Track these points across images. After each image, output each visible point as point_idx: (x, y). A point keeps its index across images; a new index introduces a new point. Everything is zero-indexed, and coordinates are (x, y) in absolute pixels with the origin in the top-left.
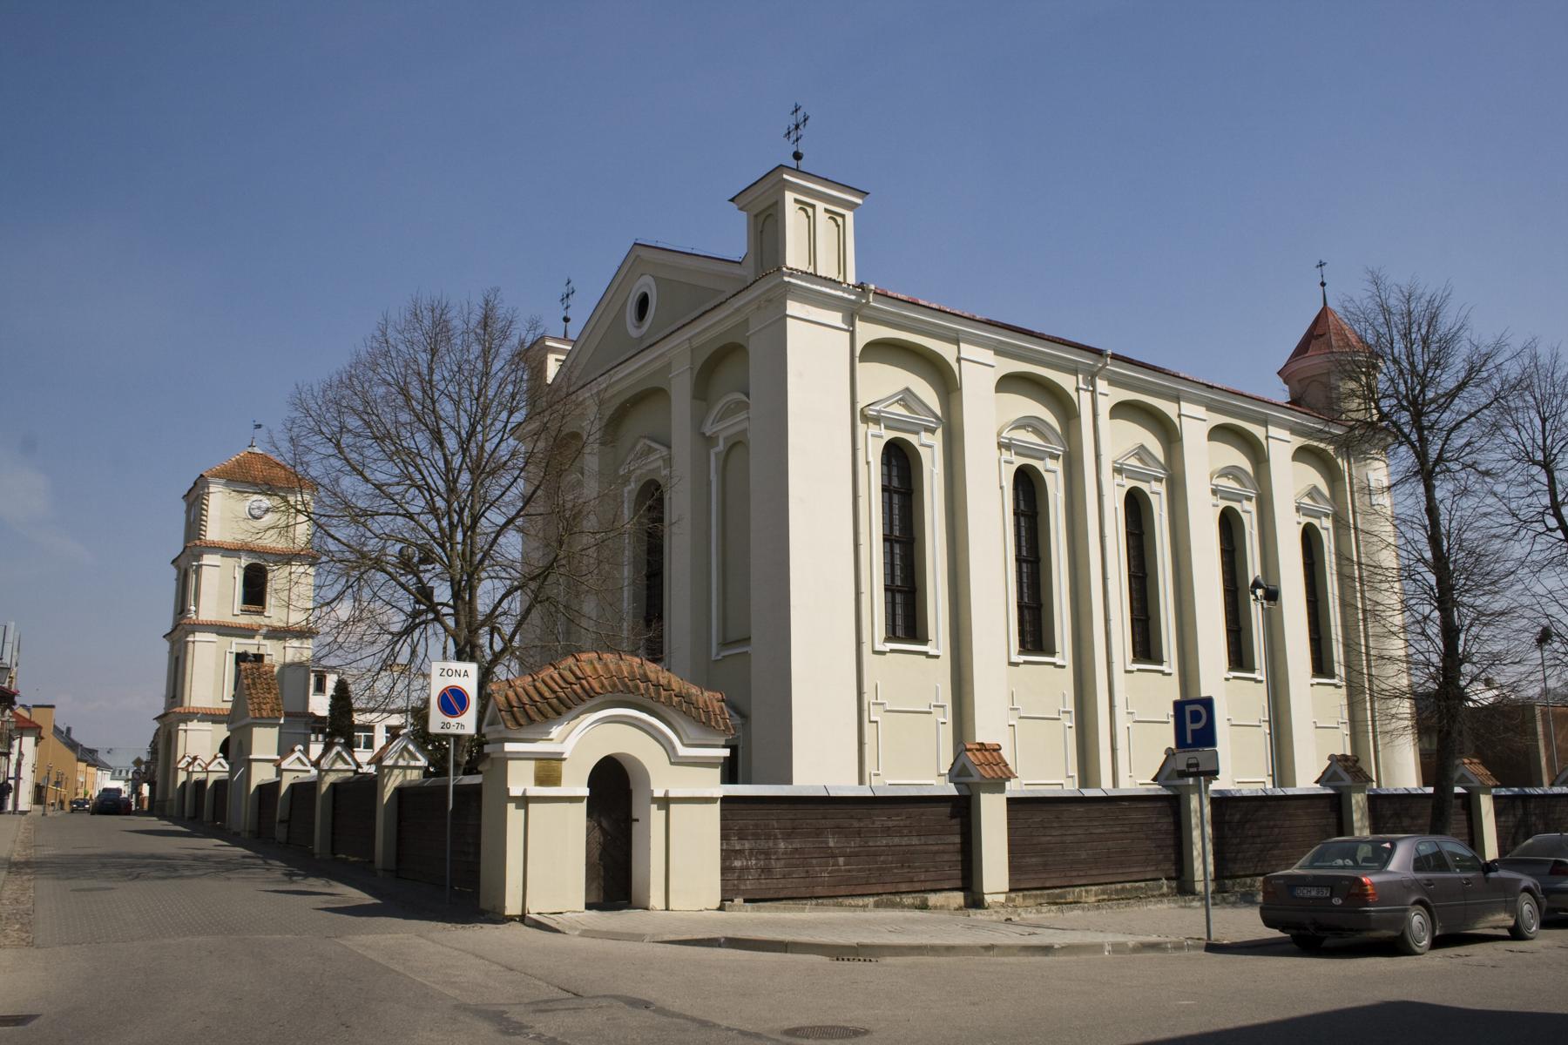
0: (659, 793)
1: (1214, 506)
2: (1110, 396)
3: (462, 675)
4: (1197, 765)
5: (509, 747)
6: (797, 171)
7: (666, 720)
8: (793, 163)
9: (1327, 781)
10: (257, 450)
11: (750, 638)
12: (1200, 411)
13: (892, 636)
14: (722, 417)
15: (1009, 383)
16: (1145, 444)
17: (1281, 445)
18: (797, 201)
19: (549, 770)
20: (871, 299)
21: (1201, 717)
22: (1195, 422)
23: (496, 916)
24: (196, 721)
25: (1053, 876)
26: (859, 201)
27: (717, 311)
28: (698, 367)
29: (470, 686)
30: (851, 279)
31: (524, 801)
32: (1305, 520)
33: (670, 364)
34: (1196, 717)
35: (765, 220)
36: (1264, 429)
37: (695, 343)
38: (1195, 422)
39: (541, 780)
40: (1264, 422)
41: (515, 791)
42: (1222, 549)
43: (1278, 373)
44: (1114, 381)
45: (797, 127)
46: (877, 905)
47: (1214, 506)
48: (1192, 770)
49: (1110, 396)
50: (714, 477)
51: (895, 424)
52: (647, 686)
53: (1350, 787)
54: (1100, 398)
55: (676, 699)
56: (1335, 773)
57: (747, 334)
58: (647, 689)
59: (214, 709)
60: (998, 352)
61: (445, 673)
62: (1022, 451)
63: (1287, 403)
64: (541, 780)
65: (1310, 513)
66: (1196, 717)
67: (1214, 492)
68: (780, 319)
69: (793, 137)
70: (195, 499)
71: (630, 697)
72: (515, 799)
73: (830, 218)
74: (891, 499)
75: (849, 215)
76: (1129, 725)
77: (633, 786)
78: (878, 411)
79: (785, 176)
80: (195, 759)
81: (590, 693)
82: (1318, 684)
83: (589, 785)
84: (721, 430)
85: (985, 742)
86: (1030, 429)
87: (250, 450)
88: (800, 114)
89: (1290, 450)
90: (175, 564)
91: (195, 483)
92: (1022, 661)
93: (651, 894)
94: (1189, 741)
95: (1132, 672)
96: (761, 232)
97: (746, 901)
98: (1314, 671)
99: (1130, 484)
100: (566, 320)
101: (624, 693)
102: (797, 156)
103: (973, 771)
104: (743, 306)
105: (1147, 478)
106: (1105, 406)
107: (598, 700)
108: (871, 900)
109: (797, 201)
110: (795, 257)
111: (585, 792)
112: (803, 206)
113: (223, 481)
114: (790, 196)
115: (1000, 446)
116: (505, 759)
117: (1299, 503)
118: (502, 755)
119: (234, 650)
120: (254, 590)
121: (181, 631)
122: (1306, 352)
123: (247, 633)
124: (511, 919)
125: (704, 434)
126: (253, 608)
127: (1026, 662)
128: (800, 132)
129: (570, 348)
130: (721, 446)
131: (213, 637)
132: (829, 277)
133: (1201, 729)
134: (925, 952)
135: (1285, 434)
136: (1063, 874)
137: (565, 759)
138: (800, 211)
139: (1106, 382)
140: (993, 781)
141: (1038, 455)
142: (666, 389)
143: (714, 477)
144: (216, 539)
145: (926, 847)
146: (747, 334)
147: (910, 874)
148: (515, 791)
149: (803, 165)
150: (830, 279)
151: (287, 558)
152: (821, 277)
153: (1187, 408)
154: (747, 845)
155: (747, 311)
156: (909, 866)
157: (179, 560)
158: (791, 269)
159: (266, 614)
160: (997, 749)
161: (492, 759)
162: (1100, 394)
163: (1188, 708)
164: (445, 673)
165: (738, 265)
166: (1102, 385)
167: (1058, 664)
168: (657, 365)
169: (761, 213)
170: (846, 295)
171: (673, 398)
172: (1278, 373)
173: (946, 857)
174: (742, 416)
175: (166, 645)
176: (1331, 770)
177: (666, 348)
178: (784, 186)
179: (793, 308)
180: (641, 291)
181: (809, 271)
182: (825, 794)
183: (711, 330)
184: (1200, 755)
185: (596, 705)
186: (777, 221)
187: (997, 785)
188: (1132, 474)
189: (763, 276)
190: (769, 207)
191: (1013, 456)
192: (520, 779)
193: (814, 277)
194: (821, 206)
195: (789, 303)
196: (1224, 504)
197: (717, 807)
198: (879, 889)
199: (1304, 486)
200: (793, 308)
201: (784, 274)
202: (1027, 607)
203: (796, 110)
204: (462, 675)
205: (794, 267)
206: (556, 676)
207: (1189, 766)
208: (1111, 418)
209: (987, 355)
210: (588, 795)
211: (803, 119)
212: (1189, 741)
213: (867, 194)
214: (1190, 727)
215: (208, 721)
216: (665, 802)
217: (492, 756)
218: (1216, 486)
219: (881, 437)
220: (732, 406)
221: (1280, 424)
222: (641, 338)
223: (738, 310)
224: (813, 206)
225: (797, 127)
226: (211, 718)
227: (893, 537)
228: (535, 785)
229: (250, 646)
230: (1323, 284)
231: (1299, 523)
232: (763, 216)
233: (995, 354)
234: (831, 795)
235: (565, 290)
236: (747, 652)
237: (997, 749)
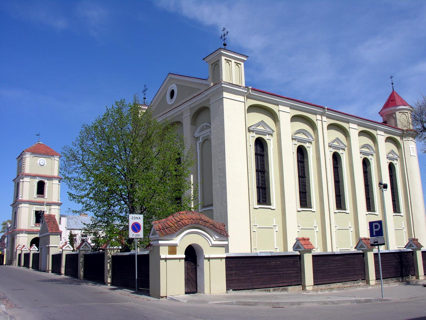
0: (207, 256)
1: (361, 157)
2: (328, 122)
3: (138, 219)
4: (377, 242)
5: (160, 242)
6: (225, 49)
7: (206, 231)
8: (223, 47)
9: (408, 247)
10: (41, 143)
11: (213, 204)
12: (355, 126)
13: (259, 202)
14: (201, 131)
15: (295, 118)
16: (393, 150)
17: (381, 136)
18: (225, 59)
19: (173, 249)
20: (250, 92)
21: (377, 228)
22: (354, 129)
23: (159, 297)
24: (24, 233)
25: (326, 280)
26: (245, 59)
27: (199, 96)
28: (193, 113)
29: (141, 222)
30: (244, 85)
31: (166, 259)
32: (389, 161)
33: (182, 113)
34: (376, 227)
35: (215, 66)
36: (376, 131)
37: (192, 106)
38: (354, 129)
39: (170, 253)
40: (376, 129)
41: (163, 256)
42: (363, 171)
43: (379, 113)
44: (328, 117)
45: (224, 35)
46: (274, 290)
47: (361, 157)
48: (375, 244)
49: (328, 122)
50: (198, 151)
51: (259, 133)
52: (202, 221)
53: (416, 249)
54: (324, 123)
55: (211, 226)
56: (411, 244)
57: (210, 104)
58: (202, 223)
59: (29, 229)
60: (358, 125)
61: (133, 218)
62: (299, 140)
63: (382, 123)
64: (170, 253)
65: (391, 159)
66: (376, 227)
67: (361, 153)
68: (221, 98)
69: (223, 38)
70: (20, 159)
71: (197, 225)
72: (163, 259)
73: (236, 65)
74: (257, 157)
75: (242, 64)
76: (336, 231)
77: (197, 254)
78: (254, 129)
79: (222, 51)
80: (24, 246)
81: (185, 225)
82: (395, 215)
83: (186, 254)
84: (202, 135)
85: (304, 237)
86: (366, 148)
87: (38, 143)
88: (225, 31)
89: (384, 138)
90: (14, 181)
91: (21, 154)
92: (337, 212)
93: (205, 289)
94: (374, 234)
95: (336, 213)
96: (214, 70)
97: (233, 290)
98: (394, 211)
99: (334, 151)
100: (145, 98)
101: (197, 224)
102: (225, 45)
103: (301, 246)
104: (208, 94)
105: (339, 148)
106: (325, 125)
107: (187, 226)
108: (271, 289)
109: (225, 59)
110: (225, 78)
111: (184, 256)
112: (228, 61)
113: (30, 153)
114: (223, 58)
115: (293, 139)
116: (159, 246)
117: (388, 156)
118: (158, 245)
119: (34, 209)
120: (41, 188)
121: (16, 204)
122: (388, 106)
123: (41, 204)
124: (162, 297)
125: (195, 137)
126: (41, 195)
127: (302, 211)
128: (225, 37)
129: (147, 108)
130: (201, 140)
131: (27, 205)
132: (237, 84)
133: (378, 231)
134: (247, 303)
135: (382, 133)
136: (329, 279)
137: (178, 246)
138: (227, 63)
139: (289, 108)
140: (308, 250)
141: (392, 159)
142: (182, 122)
143: (198, 151)
144: (28, 173)
145: (287, 272)
146: (210, 104)
147: (283, 281)
148: (163, 256)
149: (226, 47)
150: (237, 85)
151: (50, 178)
152: (234, 84)
153: (351, 125)
154: (234, 272)
155: (209, 96)
156: (283, 278)
157: (16, 180)
158: (225, 82)
159: (45, 198)
160: (308, 239)
161: (153, 246)
162: (324, 121)
163: (374, 224)
164: (133, 218)
165: (206, 81)
166: (324, 118)
167: (347, 213)
168: (179, 113)
169: (213, 63)
170: (243, 91)
171: (184, 124)
172: (379, 113)
173: (294, 275)
174: (208, 130)
175: (11, 208)
176: (410, 244)
177: (181, 108)
178: (221, 54)
179: (225, 94)
180: (171, 89)
181: (230, 83)
182: (257, 255)
183: (197, 102)
184: (379, 239)
185: (189, 227)
186: (219, 66)
187: (309, 251)
188: (334, 147)
189: (216, 84)
190: (216, 62)
191: (297, 142)
192: (164, 253)
193: (232, 85)
194: (233, 61)
195: (224, 93)
196: (364, 156)
197: (224, 260)
198: (274, 285)
199: (389, 150)
200: (225, 94)
201: (222, 84)
202: (302, 192)
203: (224, 30)
204: (138, 219)
205: (226, 81)
206: (173, 220)
207: (375, 242)
208: (359, 136)
209: (288, 109)
210: (185, 257)
211: (226, 33)
212: (374, 234)
213: (248, 57)
214: (375, 230)
215: (26, 234)
216: (209, 259)
217: (153, 245)
218: (361, 151)
219: (254, 137)
220: (204, 127)
221: (381, 130)
222: (172, 105)
223: (206, 96)
224: (231, 61)
225: (224, 35)
226: (28, 232)
227: (259, 170)
228: (169, 254)
229: (39, 208)
230: (392, 84)
231: (388, 162)
232: (214, 65)
233: (326, 118)
234: (258, 256)
235: (144, 88)
236: (211, 209)
237: (308, 239)
